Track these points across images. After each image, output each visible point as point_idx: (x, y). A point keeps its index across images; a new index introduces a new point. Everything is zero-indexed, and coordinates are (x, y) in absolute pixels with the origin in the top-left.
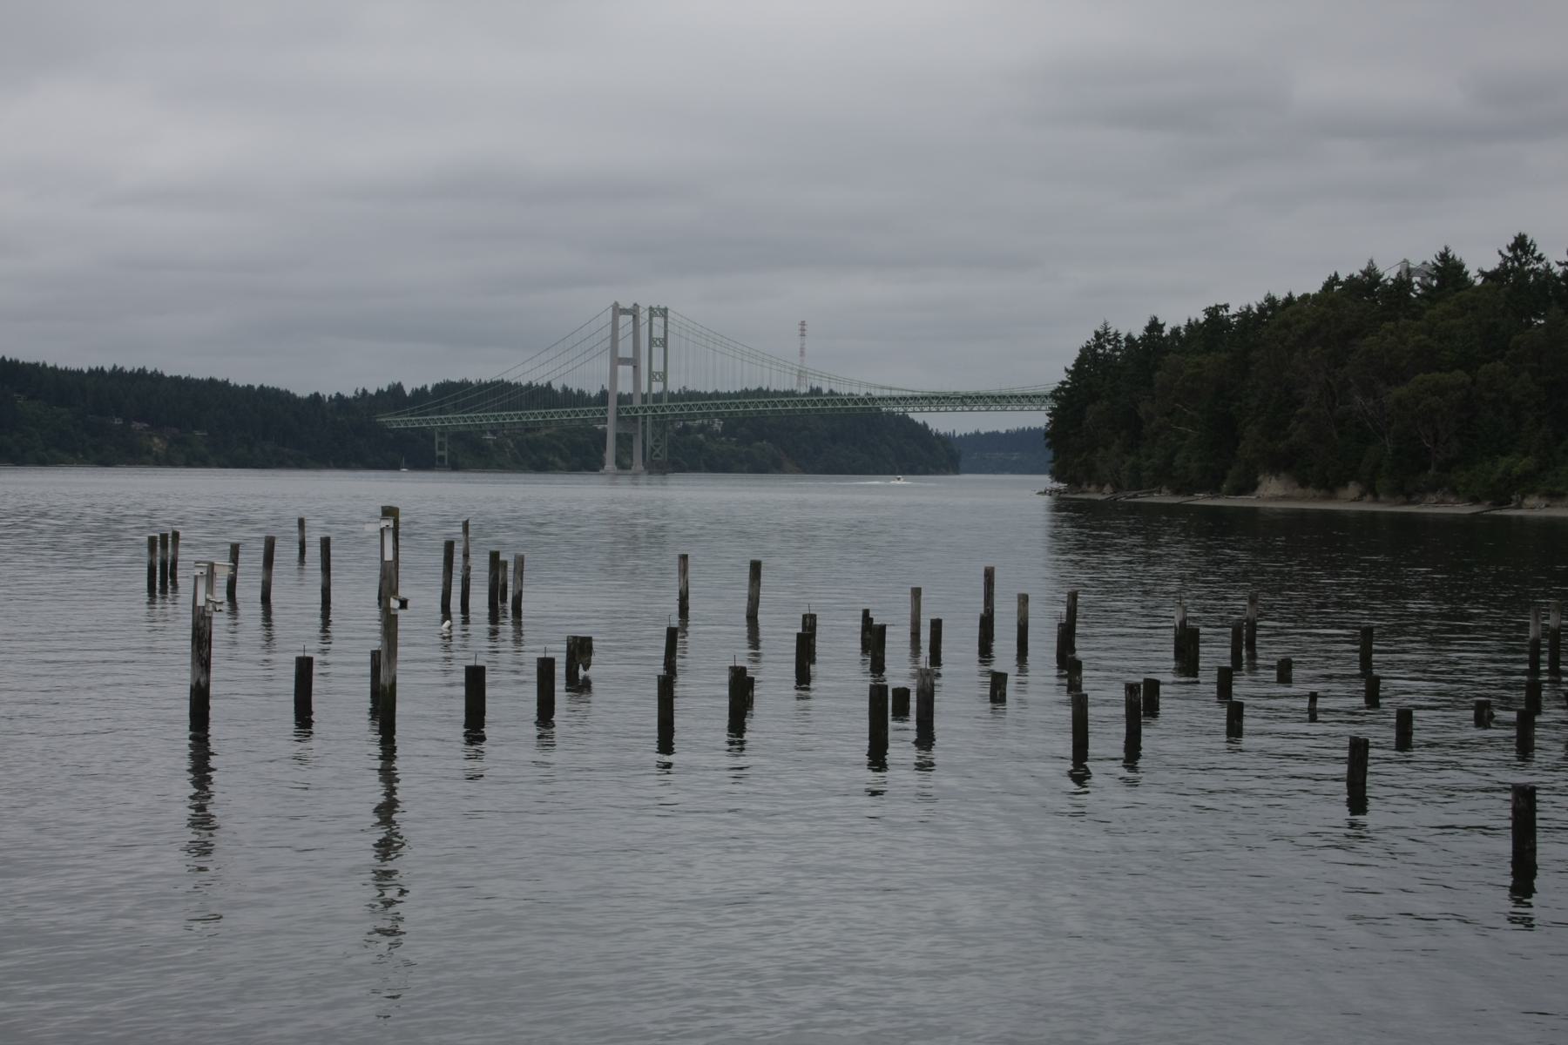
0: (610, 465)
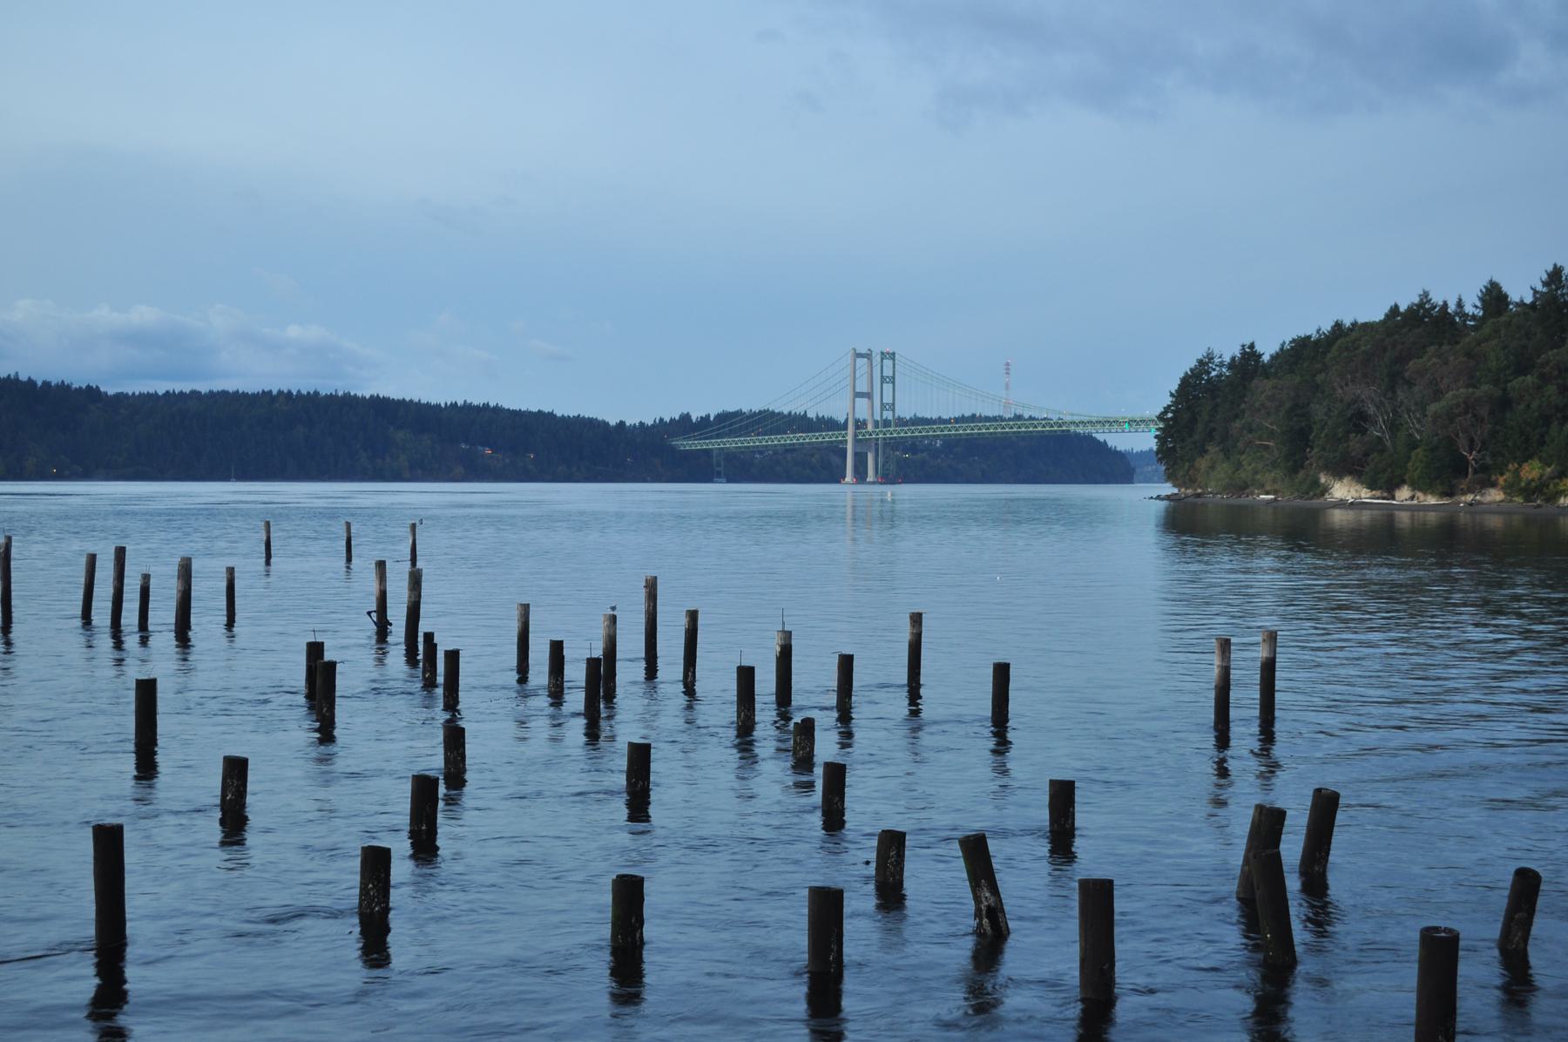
0: (849, 478)
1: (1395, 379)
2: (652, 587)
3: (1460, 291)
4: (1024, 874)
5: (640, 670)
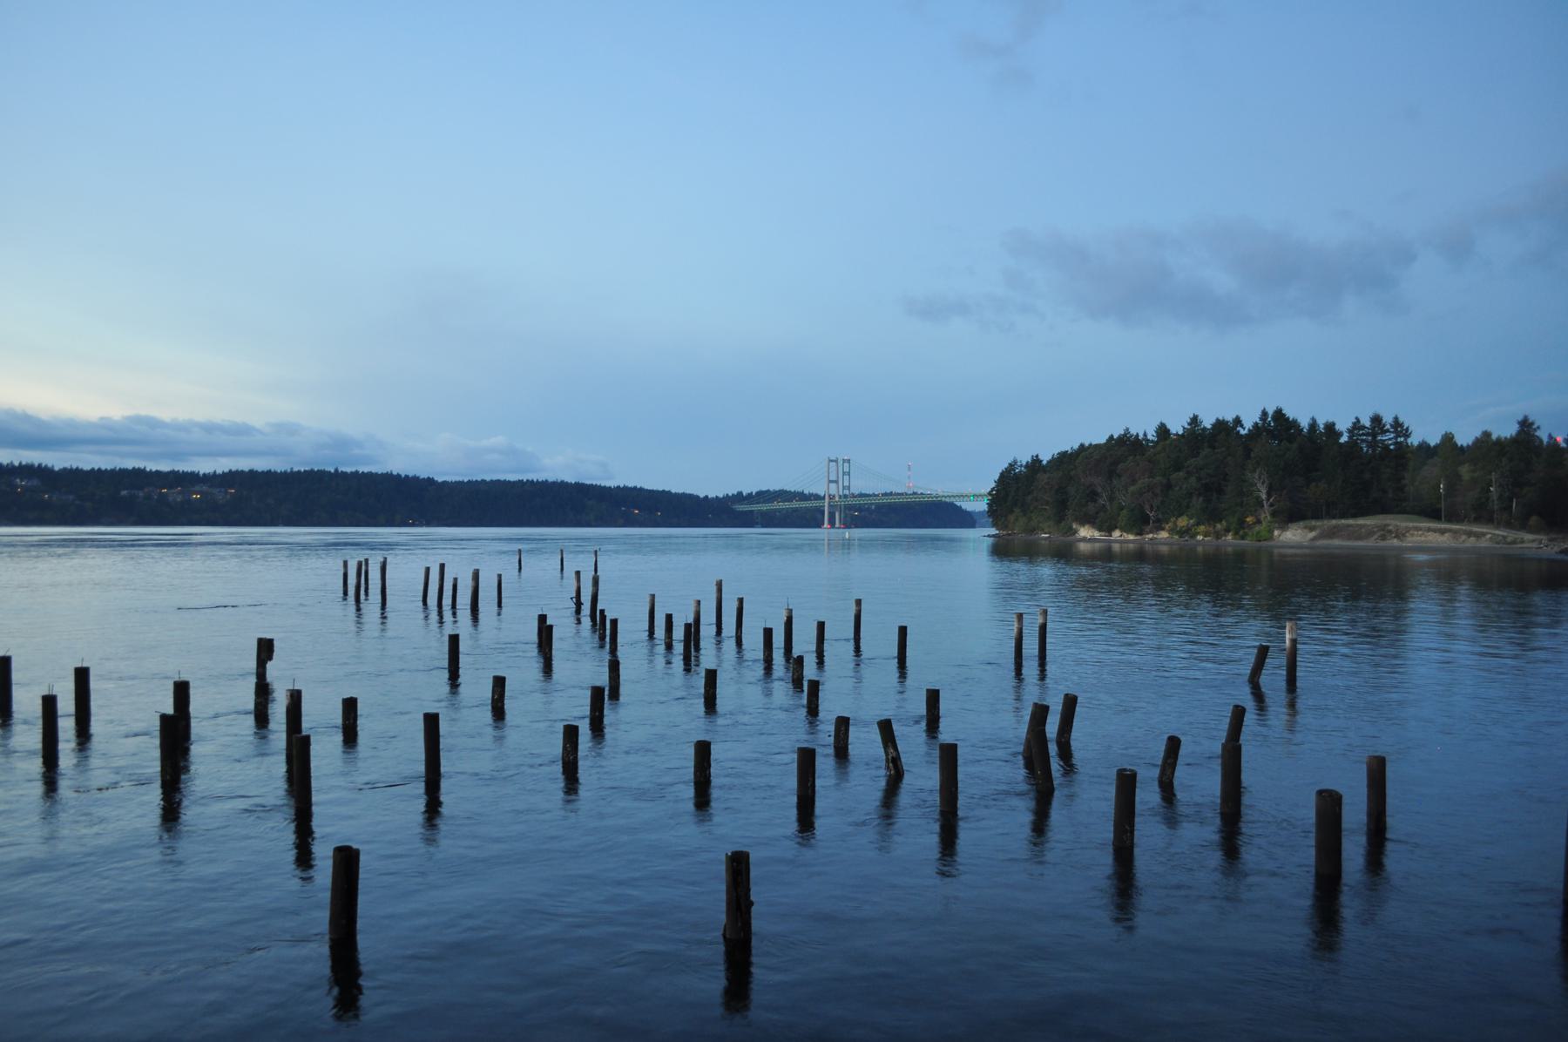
1: (1111, 474)
2: (719, 585)
3: (1145, 428)
4: (912, 740)
5: (714, 629)
